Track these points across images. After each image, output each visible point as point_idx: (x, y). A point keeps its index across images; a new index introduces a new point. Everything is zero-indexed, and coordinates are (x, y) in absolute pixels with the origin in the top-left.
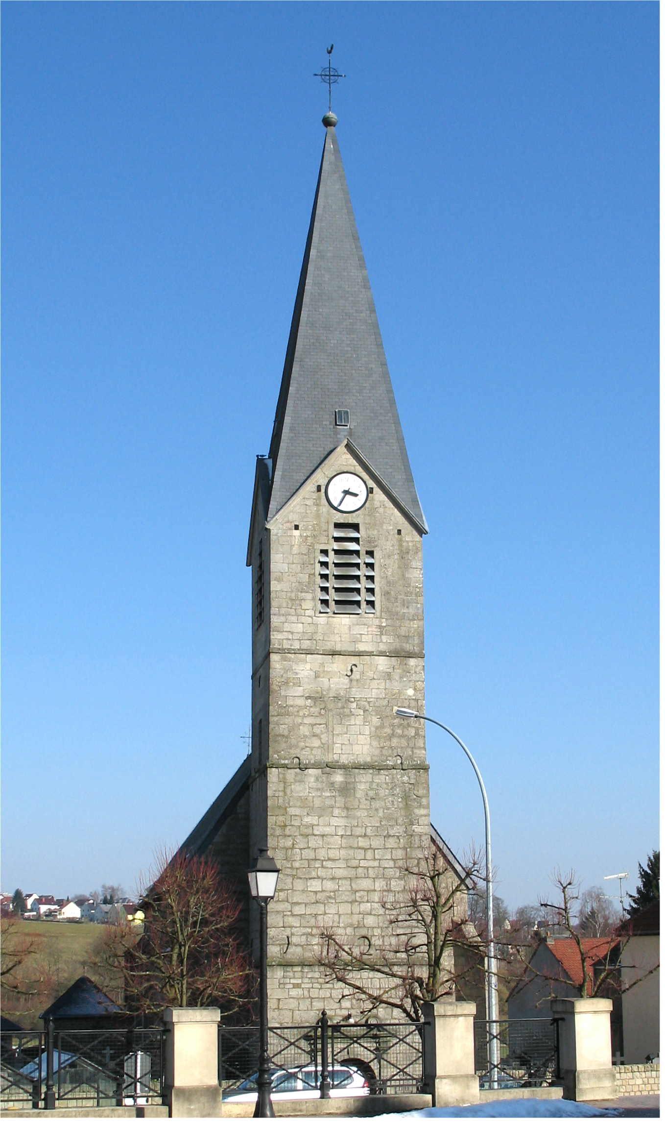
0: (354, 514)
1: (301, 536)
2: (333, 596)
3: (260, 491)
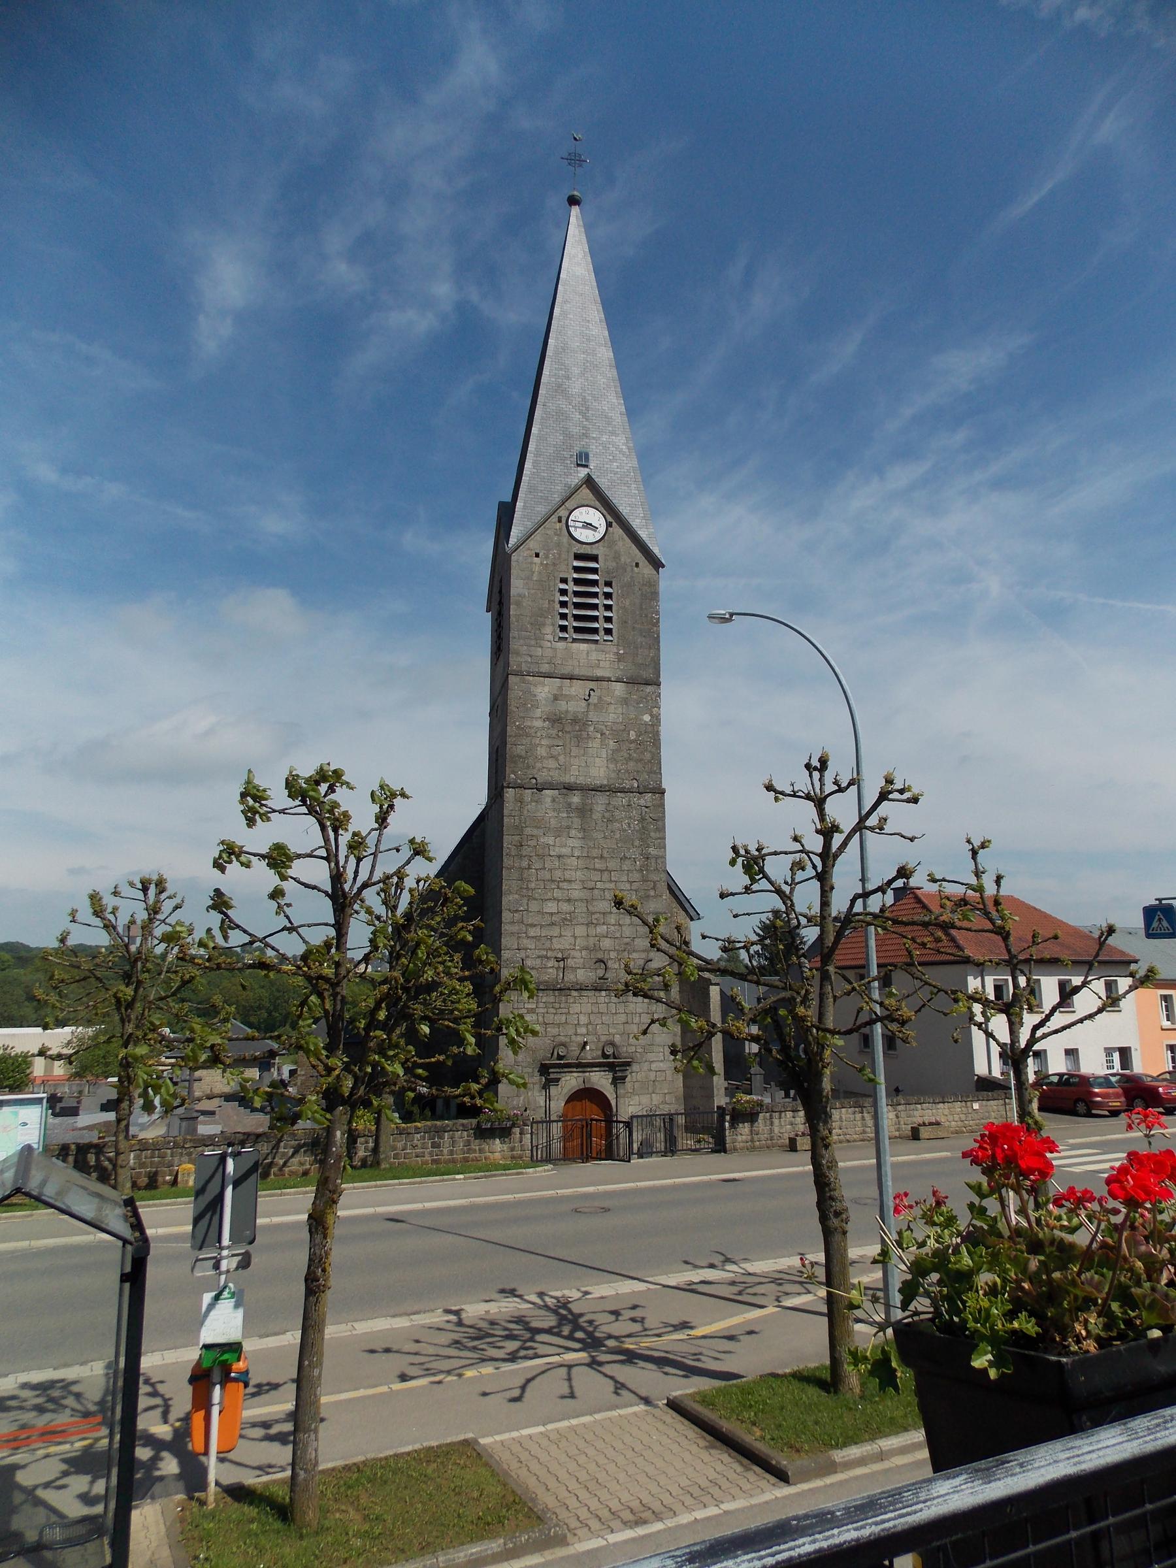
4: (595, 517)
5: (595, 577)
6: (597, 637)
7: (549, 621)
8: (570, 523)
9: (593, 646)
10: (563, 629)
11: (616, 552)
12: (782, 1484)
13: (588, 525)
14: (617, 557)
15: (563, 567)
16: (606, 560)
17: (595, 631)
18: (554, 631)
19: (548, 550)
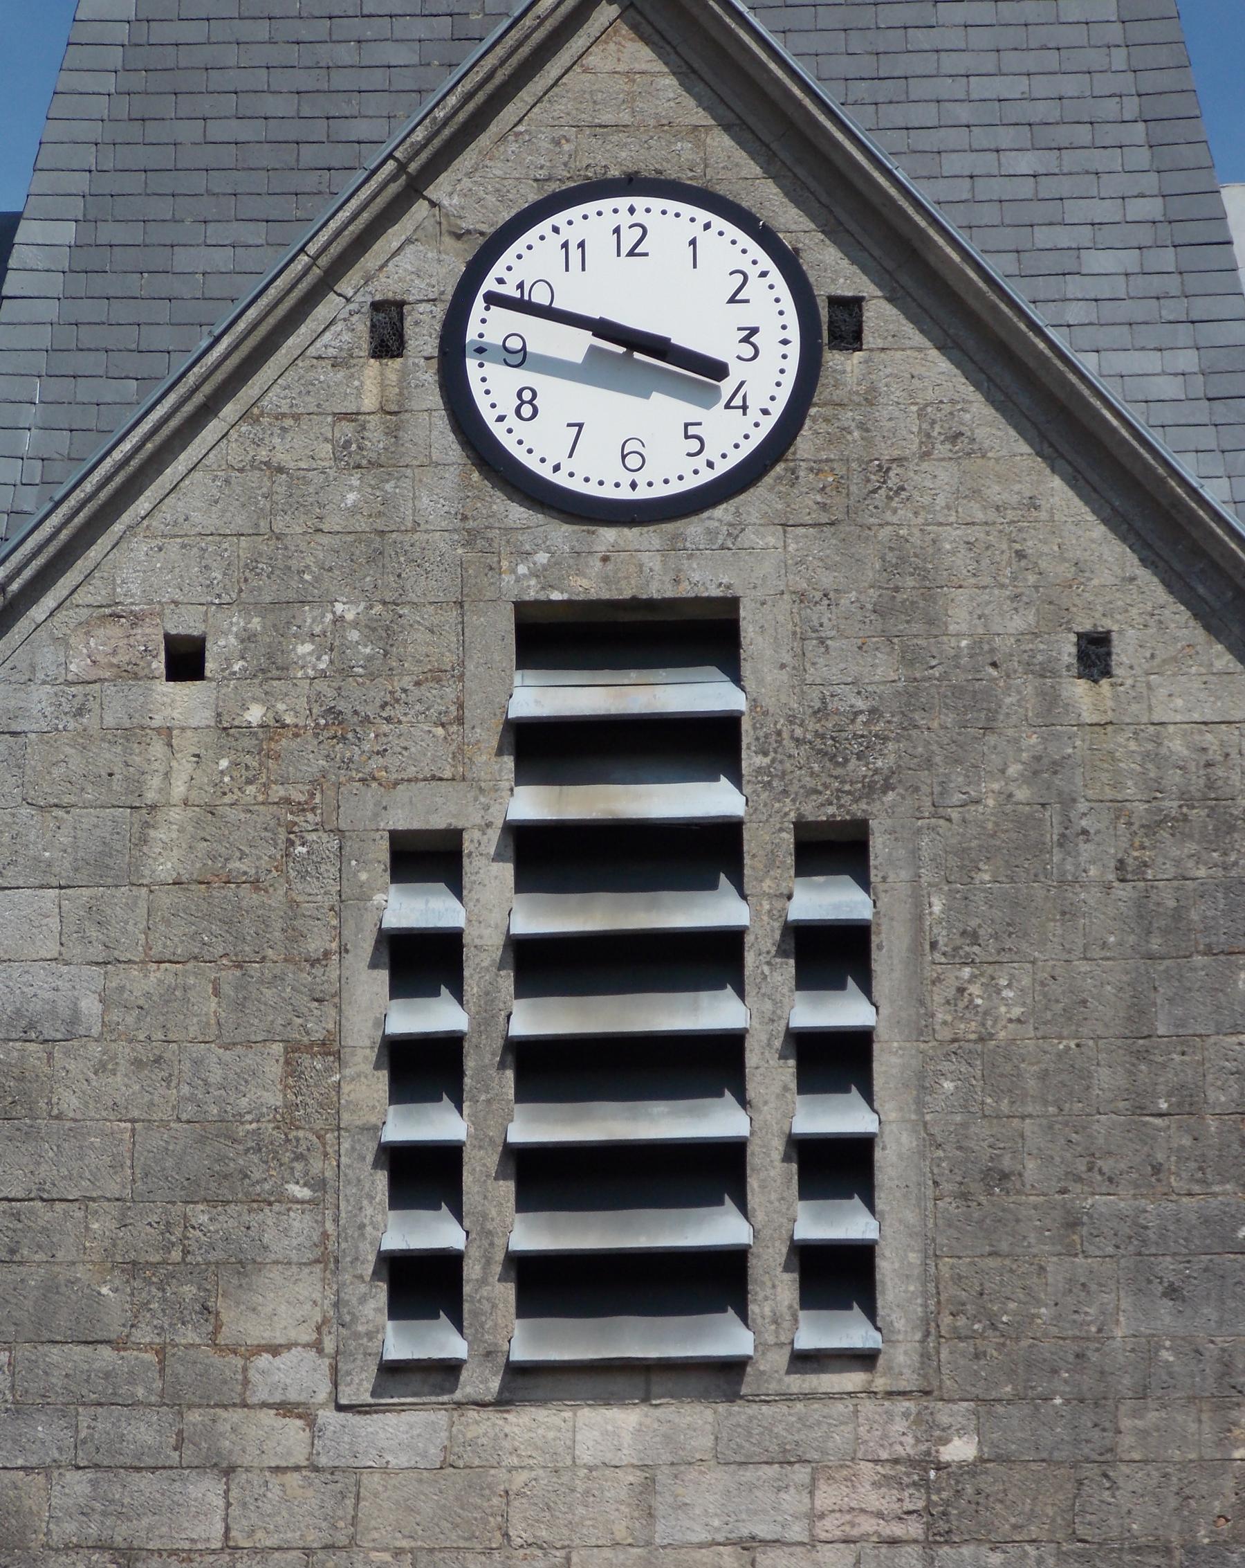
0: (693, 528)
1: (225, 729)
2: (498, 1227)
3: (1047, 352)
4: (693, 273)
5: (710, 799)
6: (727, 1338)
7: (288, 1233)
8: (486, 325)
9: (695, 1420)
10: (424, 1284)
11: (899, 559)
12: (868, 1213)
13: (638, 354)
14: (906, 600)
15: (423, 743)
16: (808, 638)
17: (717, 1279)
18: (339, 1315)
19: (282, 610)
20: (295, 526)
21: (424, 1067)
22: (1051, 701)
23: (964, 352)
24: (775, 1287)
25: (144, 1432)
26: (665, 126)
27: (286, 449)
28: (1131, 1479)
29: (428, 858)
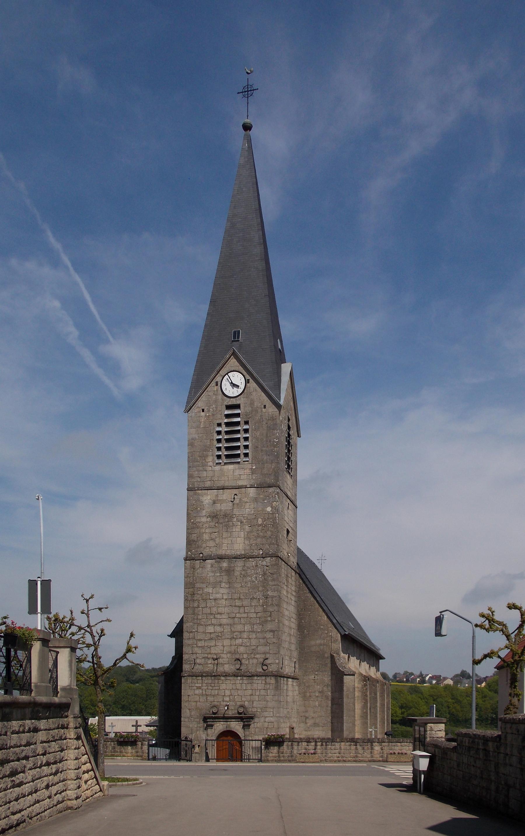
0: (237, 398)
5: (238, 419)
9: (236, 466)
10: (219, 457)
15: (219, 416)
16: (245, 407)
17: (238, 456)
20: (210, 400)
21: (219, 441)
22: (262, 410)
23: (71, 673)
24: (242, 456)
25: (201, 468)
26: (236, 366)
27: (210, 394)
28: (266, 469)
29: (219, 425)
